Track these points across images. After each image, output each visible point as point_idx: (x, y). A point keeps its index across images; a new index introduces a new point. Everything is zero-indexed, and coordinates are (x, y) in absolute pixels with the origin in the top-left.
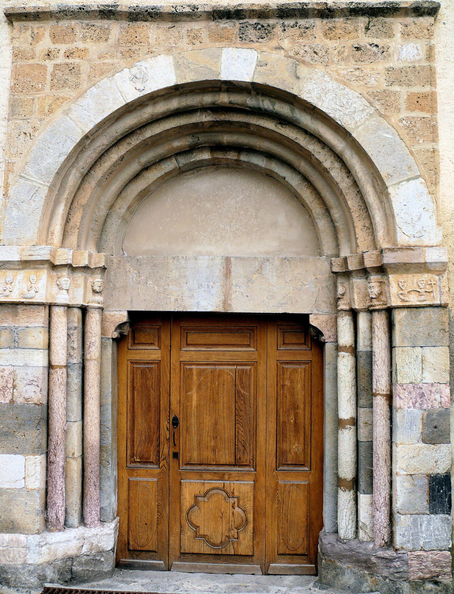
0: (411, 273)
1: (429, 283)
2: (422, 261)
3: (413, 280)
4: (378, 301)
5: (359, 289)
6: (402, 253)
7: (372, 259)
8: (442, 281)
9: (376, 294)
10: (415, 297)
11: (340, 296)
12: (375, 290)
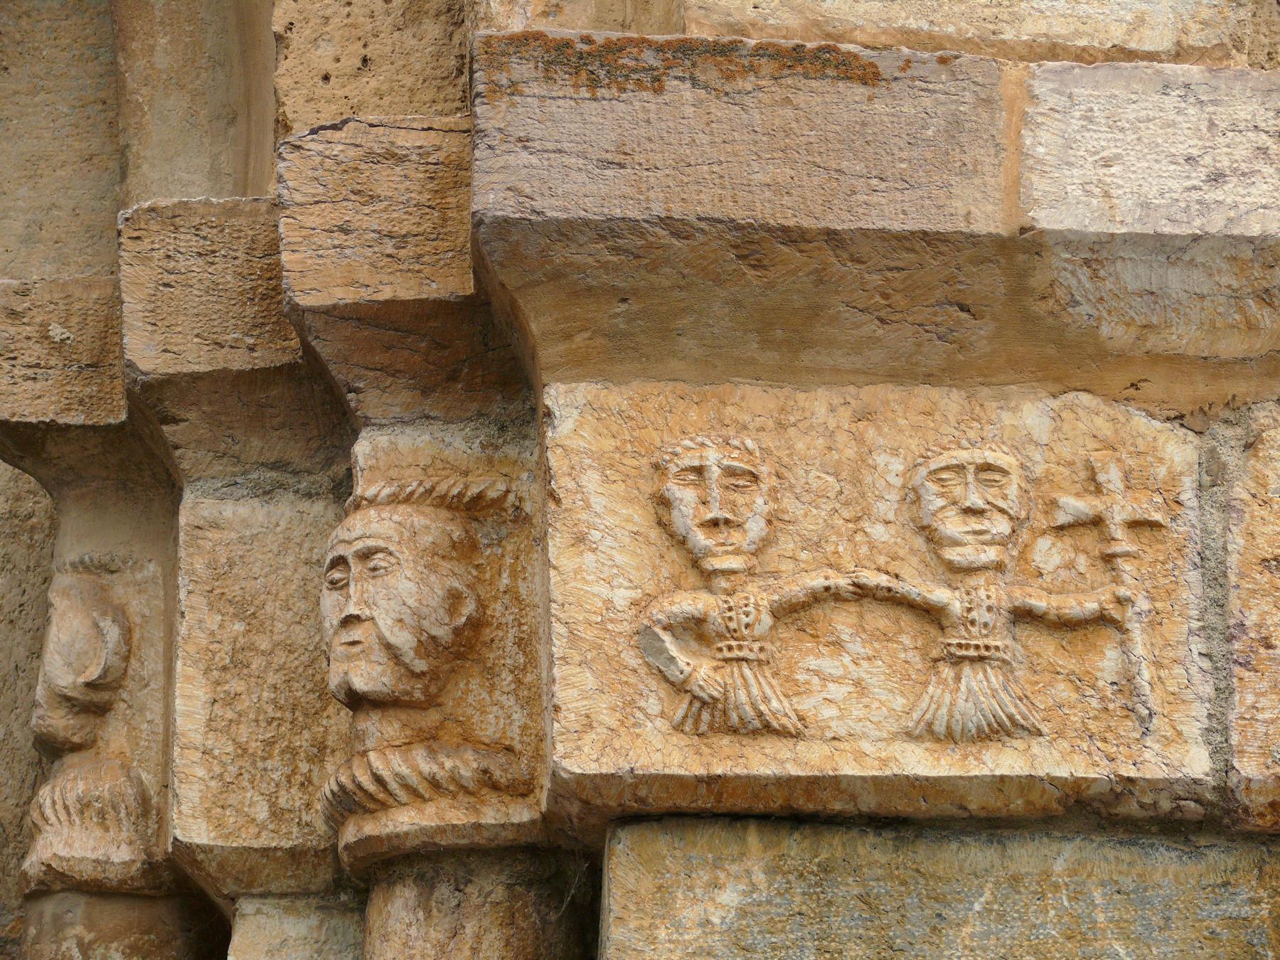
0: (835, 377)
1: (1075, 505)
2: (989, 219)
3: (864, 459)
4: (430, 739)
5: (246, 610)
6: (719, 110)
7: (368, 219)
8: (1239, 492)
9: (404, 640)
10: (873, 674)
11: (60, 722)
12: (397, 599)
